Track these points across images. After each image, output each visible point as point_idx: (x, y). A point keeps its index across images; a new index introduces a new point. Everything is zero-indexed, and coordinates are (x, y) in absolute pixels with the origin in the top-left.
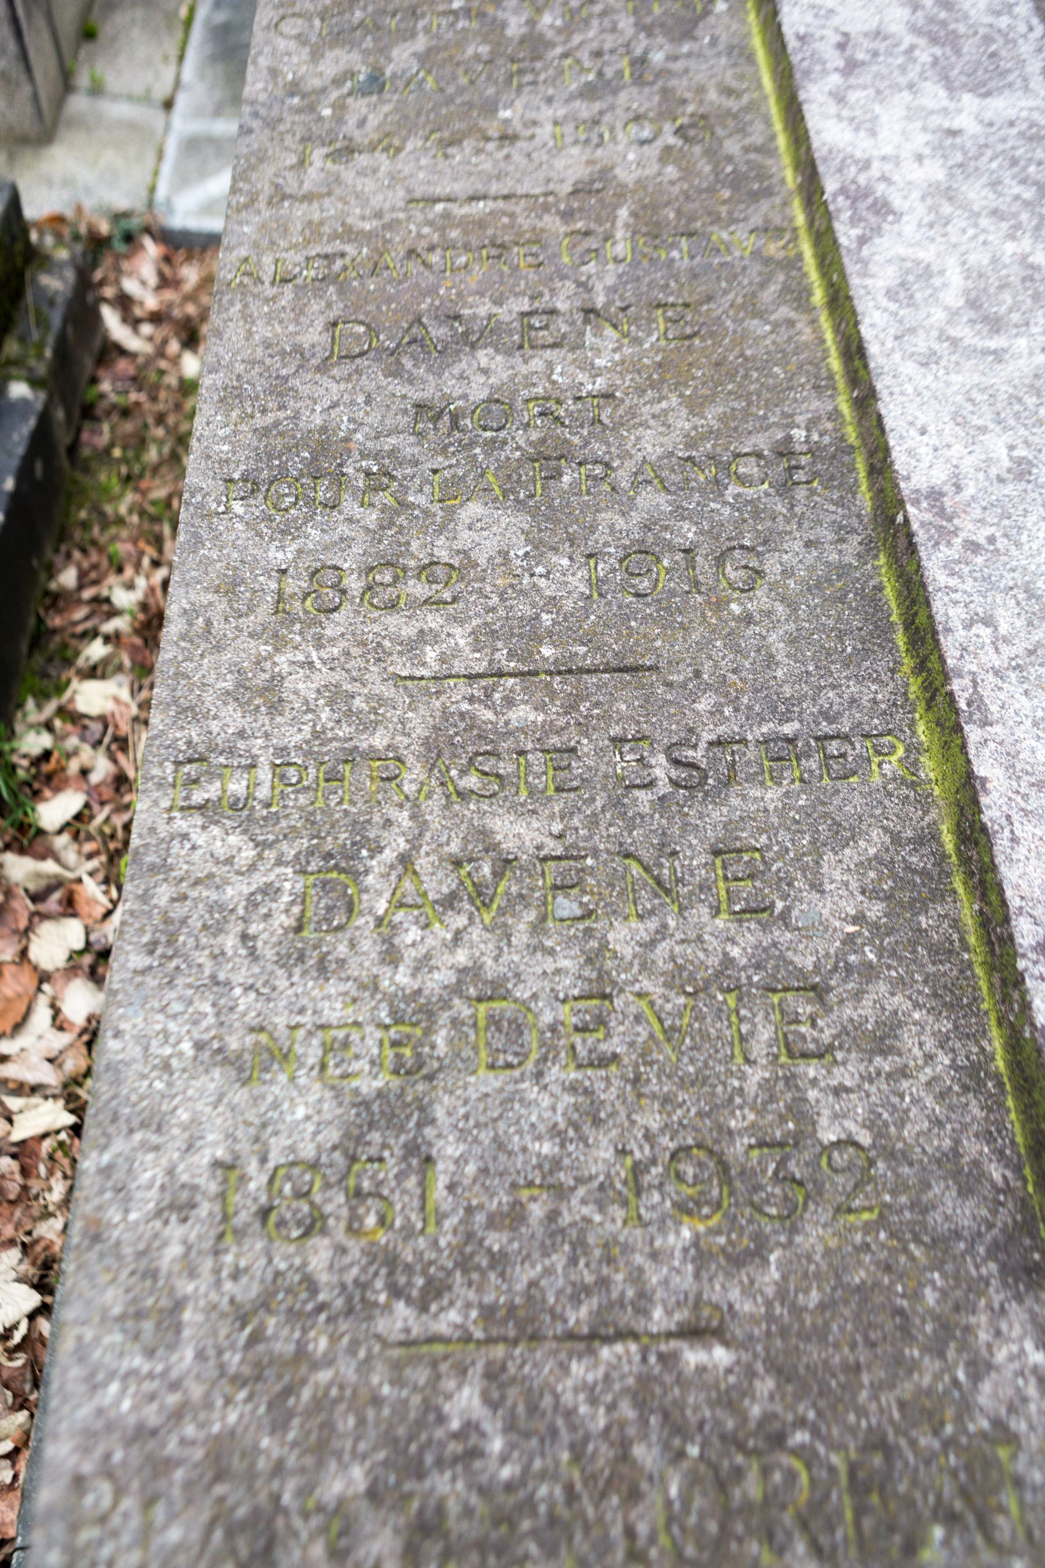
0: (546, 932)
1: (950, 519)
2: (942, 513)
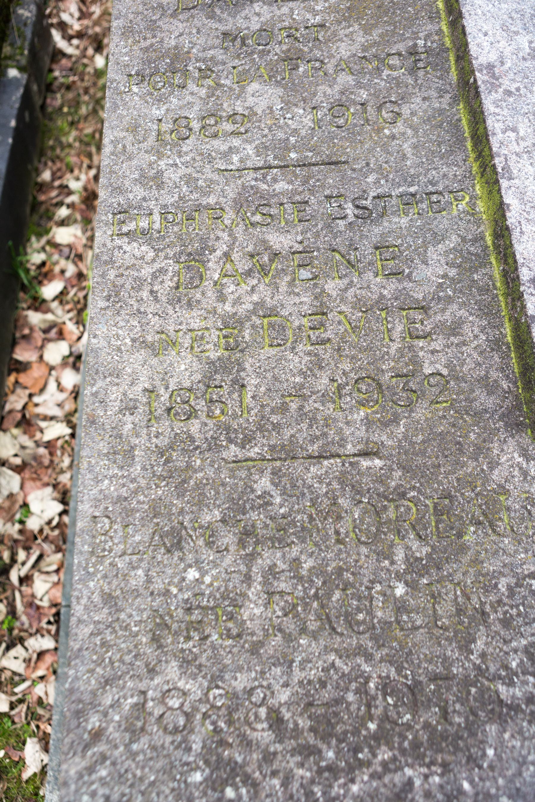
0: (295, 286)
1: (497, 79)
2: (493, 76)
